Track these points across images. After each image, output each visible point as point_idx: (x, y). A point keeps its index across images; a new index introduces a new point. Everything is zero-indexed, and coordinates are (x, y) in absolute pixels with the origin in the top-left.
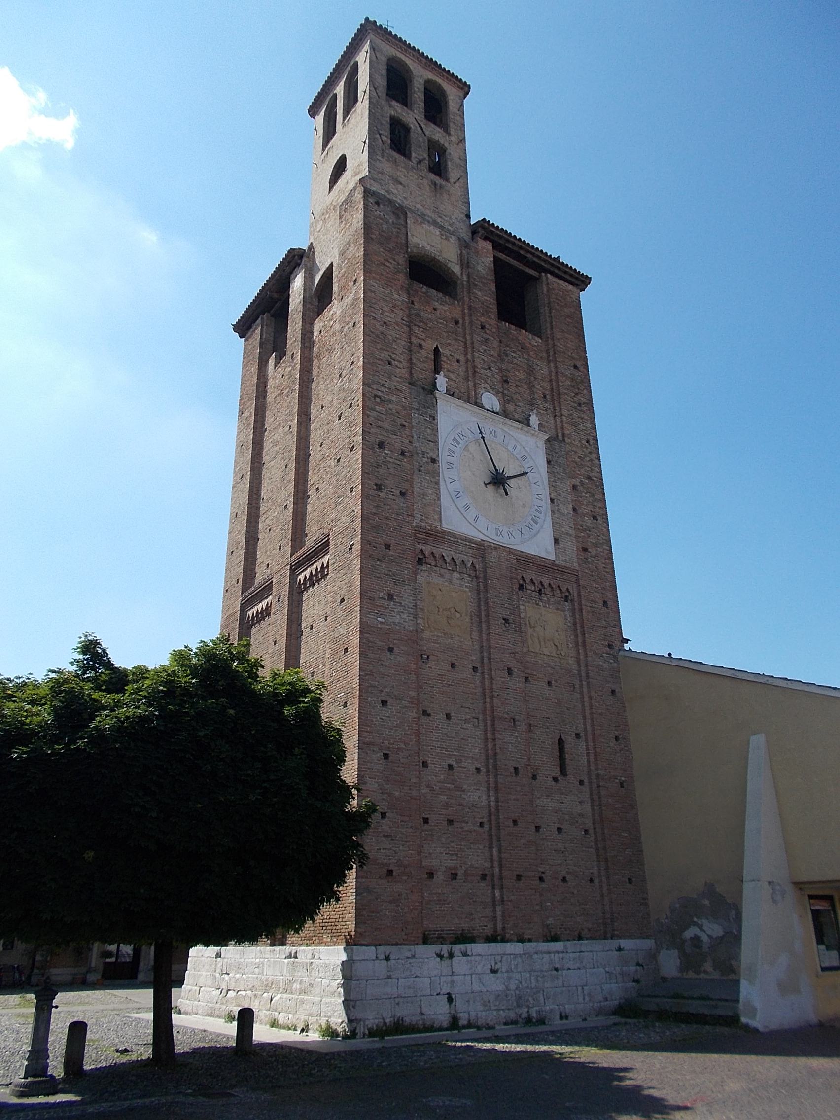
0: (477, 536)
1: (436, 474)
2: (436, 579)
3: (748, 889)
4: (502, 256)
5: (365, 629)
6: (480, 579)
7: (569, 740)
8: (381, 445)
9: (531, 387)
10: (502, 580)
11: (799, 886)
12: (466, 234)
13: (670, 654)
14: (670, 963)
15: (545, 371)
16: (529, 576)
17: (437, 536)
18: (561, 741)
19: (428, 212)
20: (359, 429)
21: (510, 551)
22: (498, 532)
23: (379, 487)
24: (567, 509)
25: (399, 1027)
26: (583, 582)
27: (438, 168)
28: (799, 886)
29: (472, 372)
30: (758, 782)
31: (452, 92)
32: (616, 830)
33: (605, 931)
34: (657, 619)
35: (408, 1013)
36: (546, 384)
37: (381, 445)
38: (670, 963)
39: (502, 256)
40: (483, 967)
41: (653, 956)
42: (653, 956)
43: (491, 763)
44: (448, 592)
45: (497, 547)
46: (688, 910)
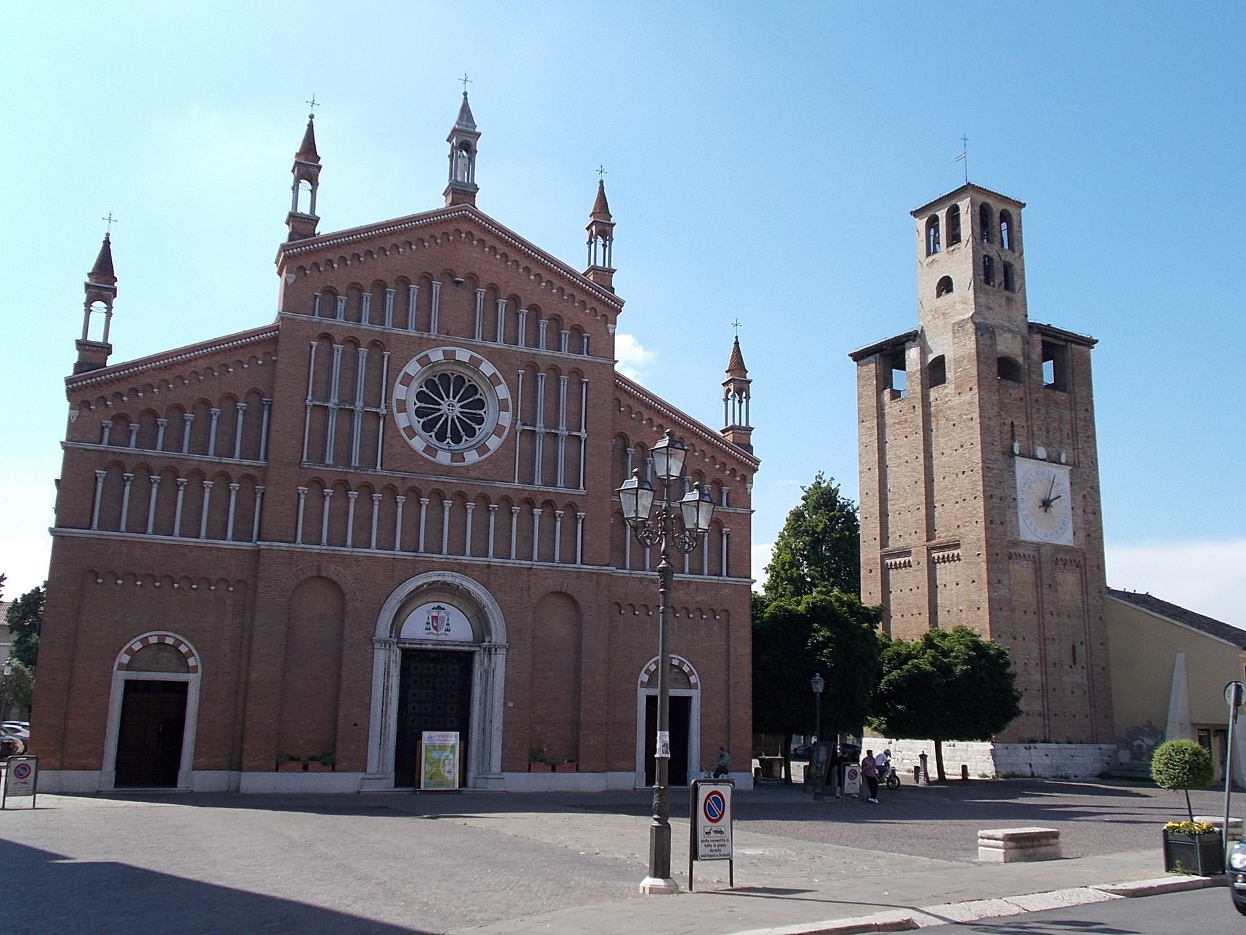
0: (1035, 540)
1: (1016, 507)
2: (1016, 566)
3: (1169, 726)
4: (1046, 338)
5: (990, 600)
6: (1037, 563)
7: (1077, 645)
8: (991, 497)
9: (1061, 430)
10: (1046, 560)
11: (1193, 725)
12: (1025, 331)
13: (959, 159)
14: (1124, 756)
15: (1068, 417)
16: (1061, 557)
17: (1017, 543)
18: (1074, 647)
19: (1006, 324)
20: (981, 488)
21: (1052, 545)
22: (1046, 535)
23: (992, 522)
24: (1080, 512)
25: (1014, 775)
26: (1087, 556)
27: (1008, 284)
28: (1193, 725)
29: (1031, 436)
30: (1179, 678)
31: (1012, 210)
32: (1099, 691)
33: (1094, 740)
34: (1125, 569)
35: (1016, 770)
36: (1068, 427)
37: (991, 497)
38: (1124, 756)
39: (1046, 338)
40: (1042, 753)
41: (1116, 752)
42: (1116, 752)
43: (1043, 659)
44: (1022, 571)
45: (1045, 544)
46: (1137, 732)
